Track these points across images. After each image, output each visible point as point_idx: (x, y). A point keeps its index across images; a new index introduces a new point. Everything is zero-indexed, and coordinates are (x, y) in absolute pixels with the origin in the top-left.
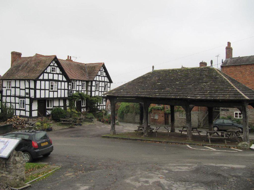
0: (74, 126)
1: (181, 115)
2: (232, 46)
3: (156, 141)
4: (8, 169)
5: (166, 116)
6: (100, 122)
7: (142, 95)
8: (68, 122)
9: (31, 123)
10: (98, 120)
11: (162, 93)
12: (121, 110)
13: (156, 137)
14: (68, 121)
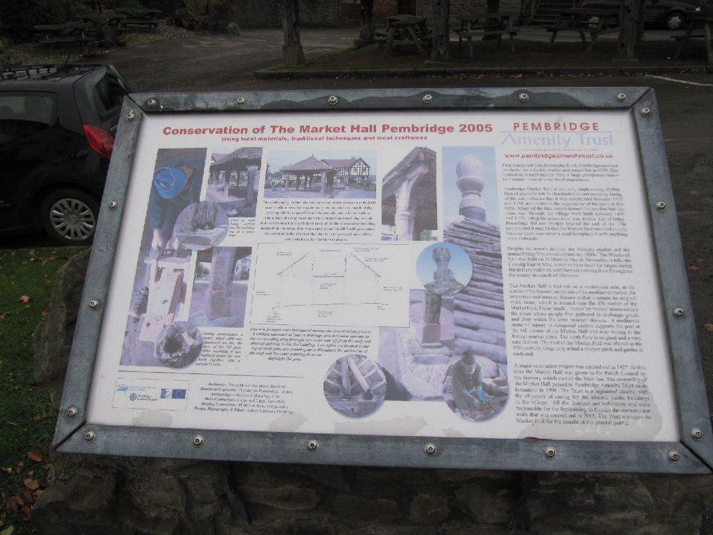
0: (99, 52)
4: (307, 63)
6: (181, 29)
8: (70, 39)
9: (308, 127)
10: (170, 24)
14: (70, 34)
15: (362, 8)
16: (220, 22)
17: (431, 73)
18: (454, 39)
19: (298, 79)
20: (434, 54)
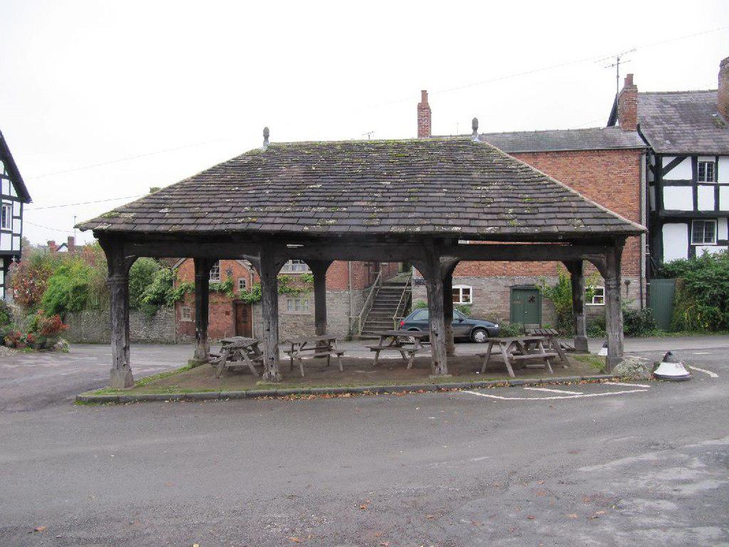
1: (299, 304)
2: (431, 101)
3: (337, 393)
5: (240, 311)
7: (267, 223)
11: (346, 218)
12: (53, 302)
13: (300, 376)
15: (197, 330)
16: (49, 340)
17: (262, 395)
18: (285, 357)
19: (125, 403)
20: (266, 375)
